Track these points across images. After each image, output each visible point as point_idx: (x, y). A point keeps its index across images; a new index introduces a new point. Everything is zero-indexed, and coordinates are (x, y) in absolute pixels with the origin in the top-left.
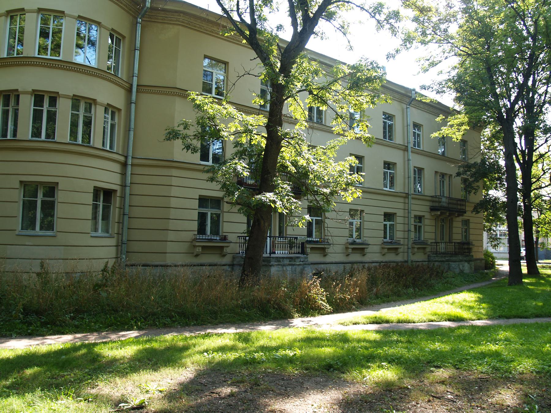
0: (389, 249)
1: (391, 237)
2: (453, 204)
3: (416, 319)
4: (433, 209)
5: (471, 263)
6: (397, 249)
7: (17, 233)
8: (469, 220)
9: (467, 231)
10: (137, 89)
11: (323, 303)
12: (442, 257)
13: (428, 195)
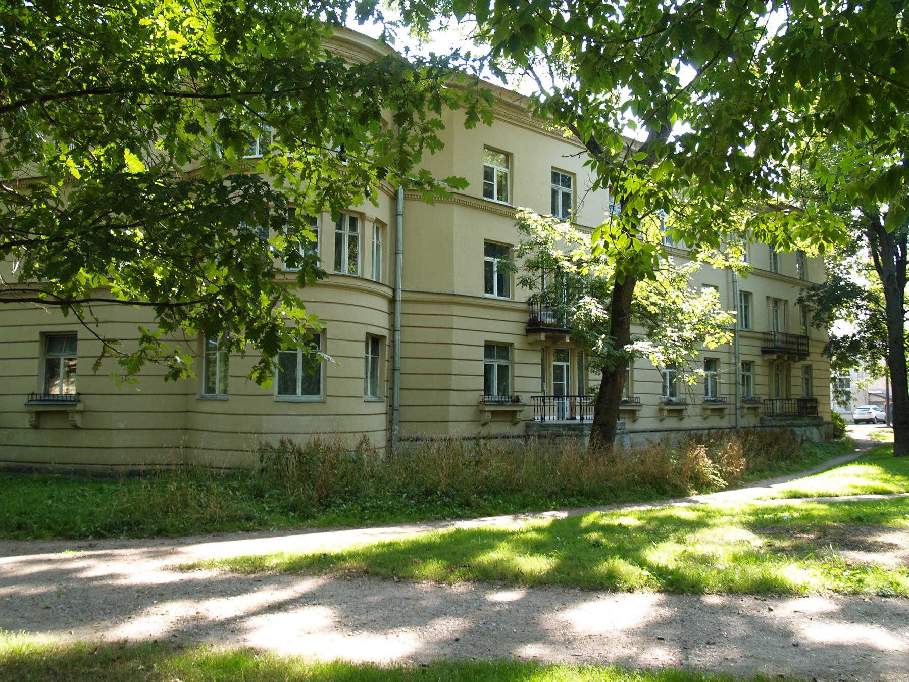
0: (713, 410)
1: (714, 392)
2: (792, 343)
3: (838, 493)
4: (765, 351)
5: (820, 428)
6: (721, 410)
7: (275, 398)
8: (811, 366)
9: (808, 382)
10: (405, 195)
11: (715, 477)
12: (781, 420)
13: (758, 331)
